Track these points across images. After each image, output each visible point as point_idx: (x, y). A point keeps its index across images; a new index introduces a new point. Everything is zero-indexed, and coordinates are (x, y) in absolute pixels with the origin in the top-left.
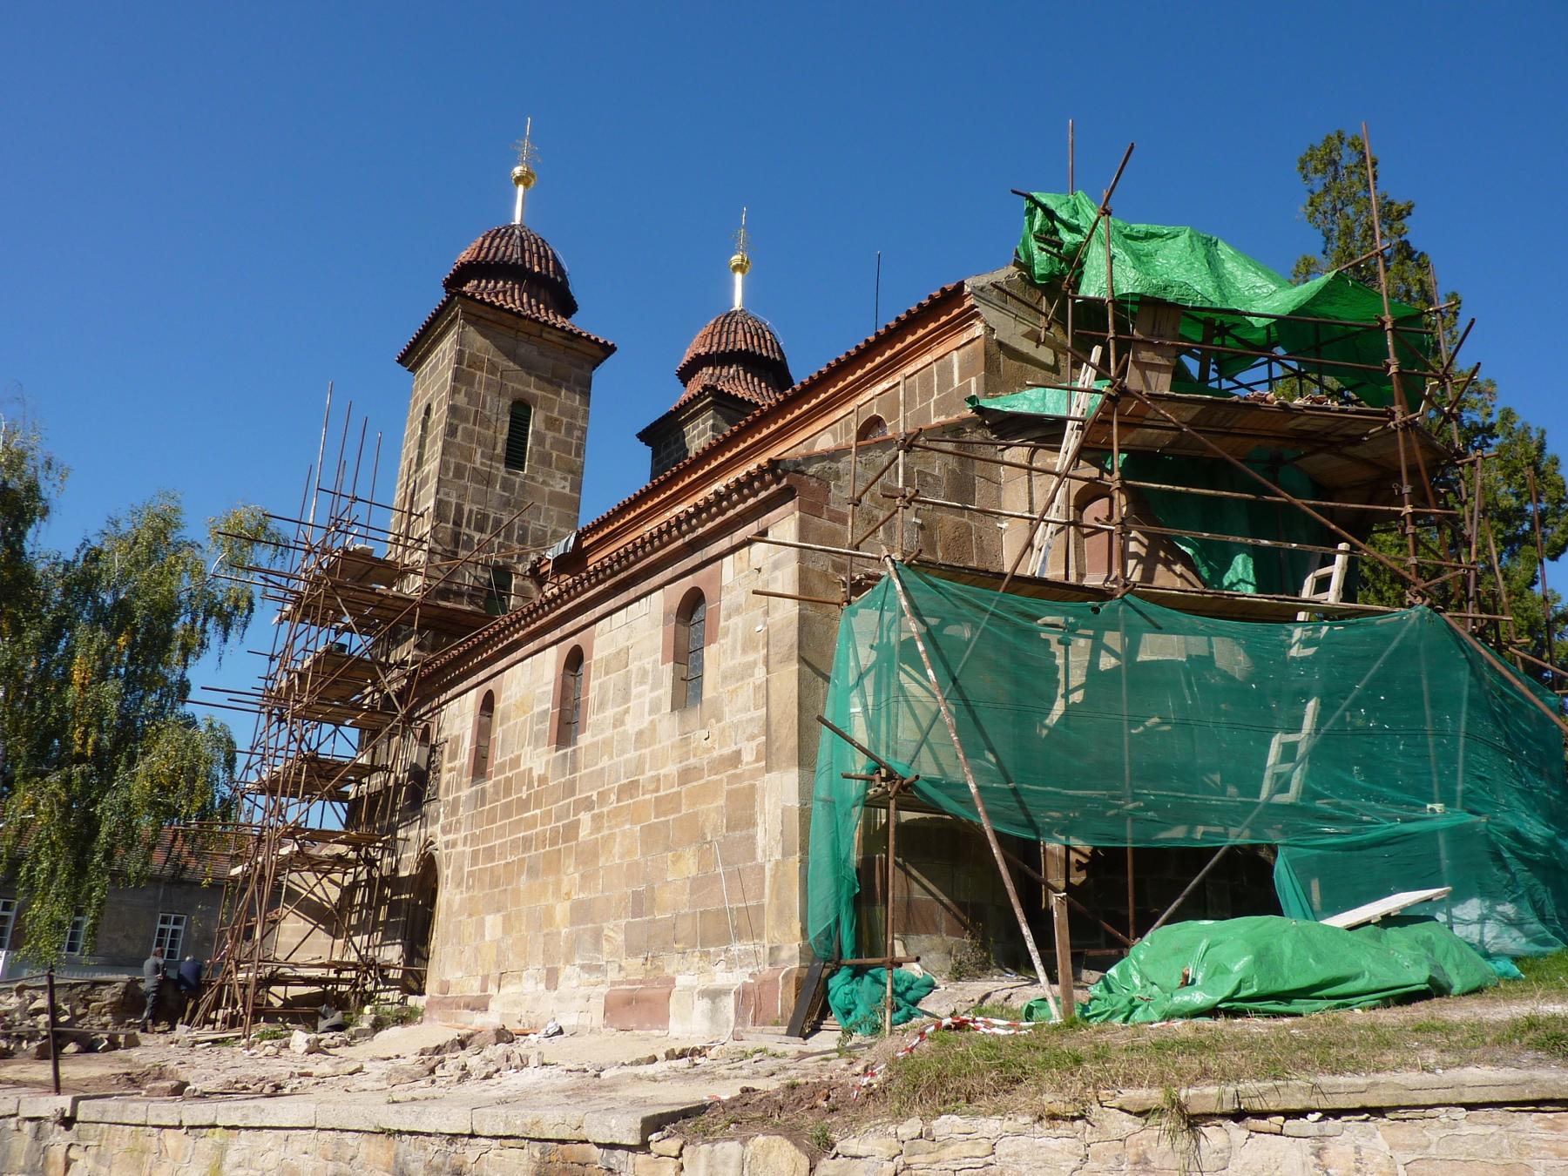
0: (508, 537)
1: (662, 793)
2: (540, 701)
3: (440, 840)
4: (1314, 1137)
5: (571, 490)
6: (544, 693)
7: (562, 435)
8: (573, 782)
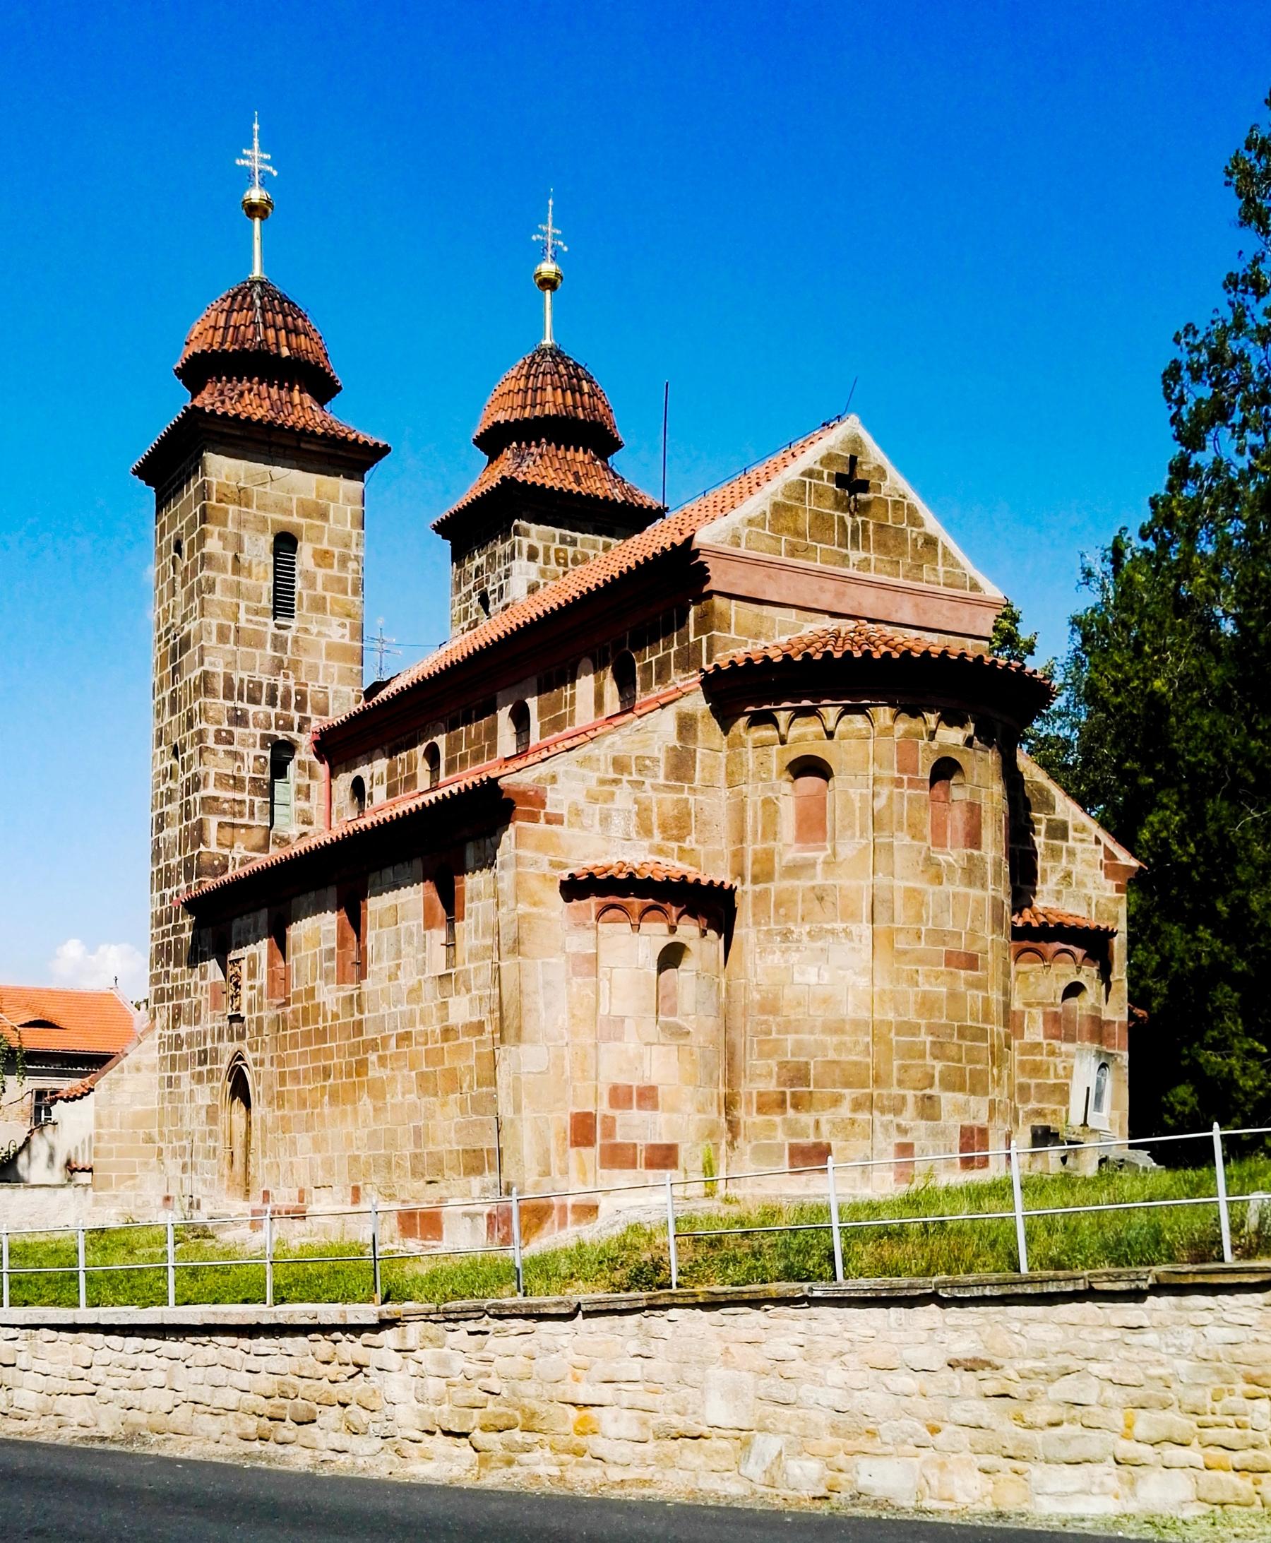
0: (286, 705)
1: (429, 1046)
2: (326, 939)
3: (249, 1057)
4: (1007, 1006)
5: (352, 638)
6: (329, 931)
7: (335, 572)
8: (360, 1022)
